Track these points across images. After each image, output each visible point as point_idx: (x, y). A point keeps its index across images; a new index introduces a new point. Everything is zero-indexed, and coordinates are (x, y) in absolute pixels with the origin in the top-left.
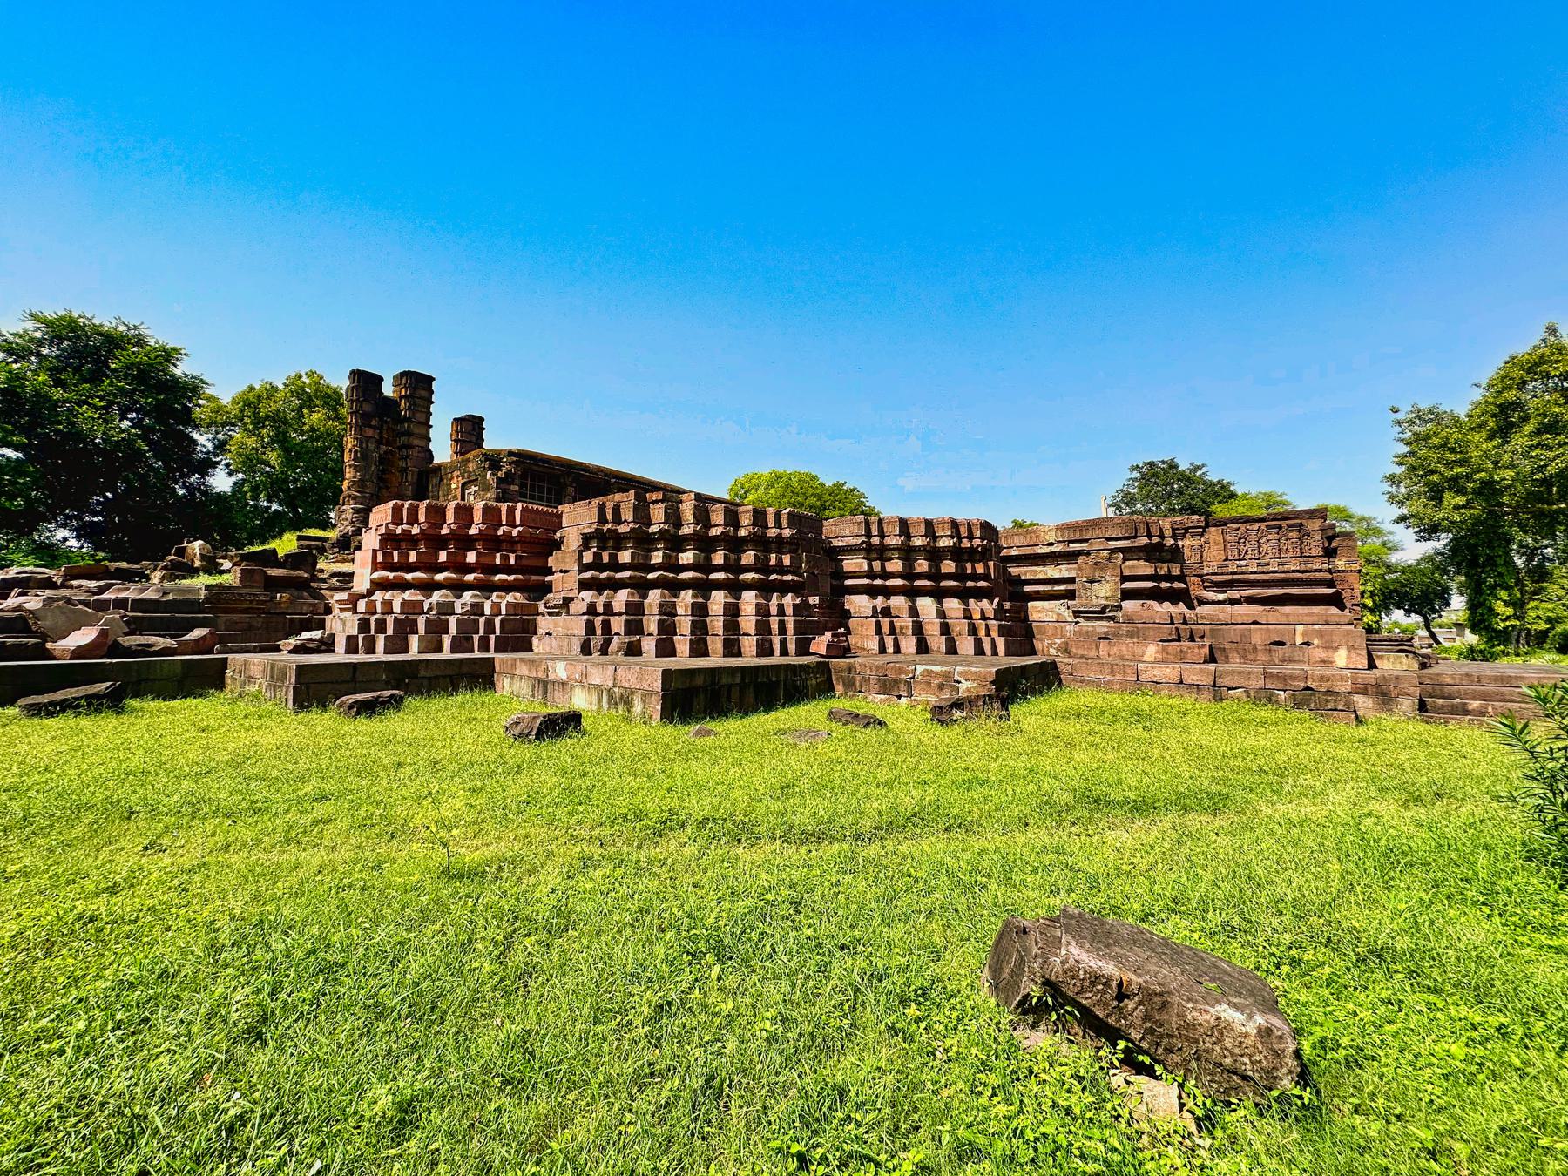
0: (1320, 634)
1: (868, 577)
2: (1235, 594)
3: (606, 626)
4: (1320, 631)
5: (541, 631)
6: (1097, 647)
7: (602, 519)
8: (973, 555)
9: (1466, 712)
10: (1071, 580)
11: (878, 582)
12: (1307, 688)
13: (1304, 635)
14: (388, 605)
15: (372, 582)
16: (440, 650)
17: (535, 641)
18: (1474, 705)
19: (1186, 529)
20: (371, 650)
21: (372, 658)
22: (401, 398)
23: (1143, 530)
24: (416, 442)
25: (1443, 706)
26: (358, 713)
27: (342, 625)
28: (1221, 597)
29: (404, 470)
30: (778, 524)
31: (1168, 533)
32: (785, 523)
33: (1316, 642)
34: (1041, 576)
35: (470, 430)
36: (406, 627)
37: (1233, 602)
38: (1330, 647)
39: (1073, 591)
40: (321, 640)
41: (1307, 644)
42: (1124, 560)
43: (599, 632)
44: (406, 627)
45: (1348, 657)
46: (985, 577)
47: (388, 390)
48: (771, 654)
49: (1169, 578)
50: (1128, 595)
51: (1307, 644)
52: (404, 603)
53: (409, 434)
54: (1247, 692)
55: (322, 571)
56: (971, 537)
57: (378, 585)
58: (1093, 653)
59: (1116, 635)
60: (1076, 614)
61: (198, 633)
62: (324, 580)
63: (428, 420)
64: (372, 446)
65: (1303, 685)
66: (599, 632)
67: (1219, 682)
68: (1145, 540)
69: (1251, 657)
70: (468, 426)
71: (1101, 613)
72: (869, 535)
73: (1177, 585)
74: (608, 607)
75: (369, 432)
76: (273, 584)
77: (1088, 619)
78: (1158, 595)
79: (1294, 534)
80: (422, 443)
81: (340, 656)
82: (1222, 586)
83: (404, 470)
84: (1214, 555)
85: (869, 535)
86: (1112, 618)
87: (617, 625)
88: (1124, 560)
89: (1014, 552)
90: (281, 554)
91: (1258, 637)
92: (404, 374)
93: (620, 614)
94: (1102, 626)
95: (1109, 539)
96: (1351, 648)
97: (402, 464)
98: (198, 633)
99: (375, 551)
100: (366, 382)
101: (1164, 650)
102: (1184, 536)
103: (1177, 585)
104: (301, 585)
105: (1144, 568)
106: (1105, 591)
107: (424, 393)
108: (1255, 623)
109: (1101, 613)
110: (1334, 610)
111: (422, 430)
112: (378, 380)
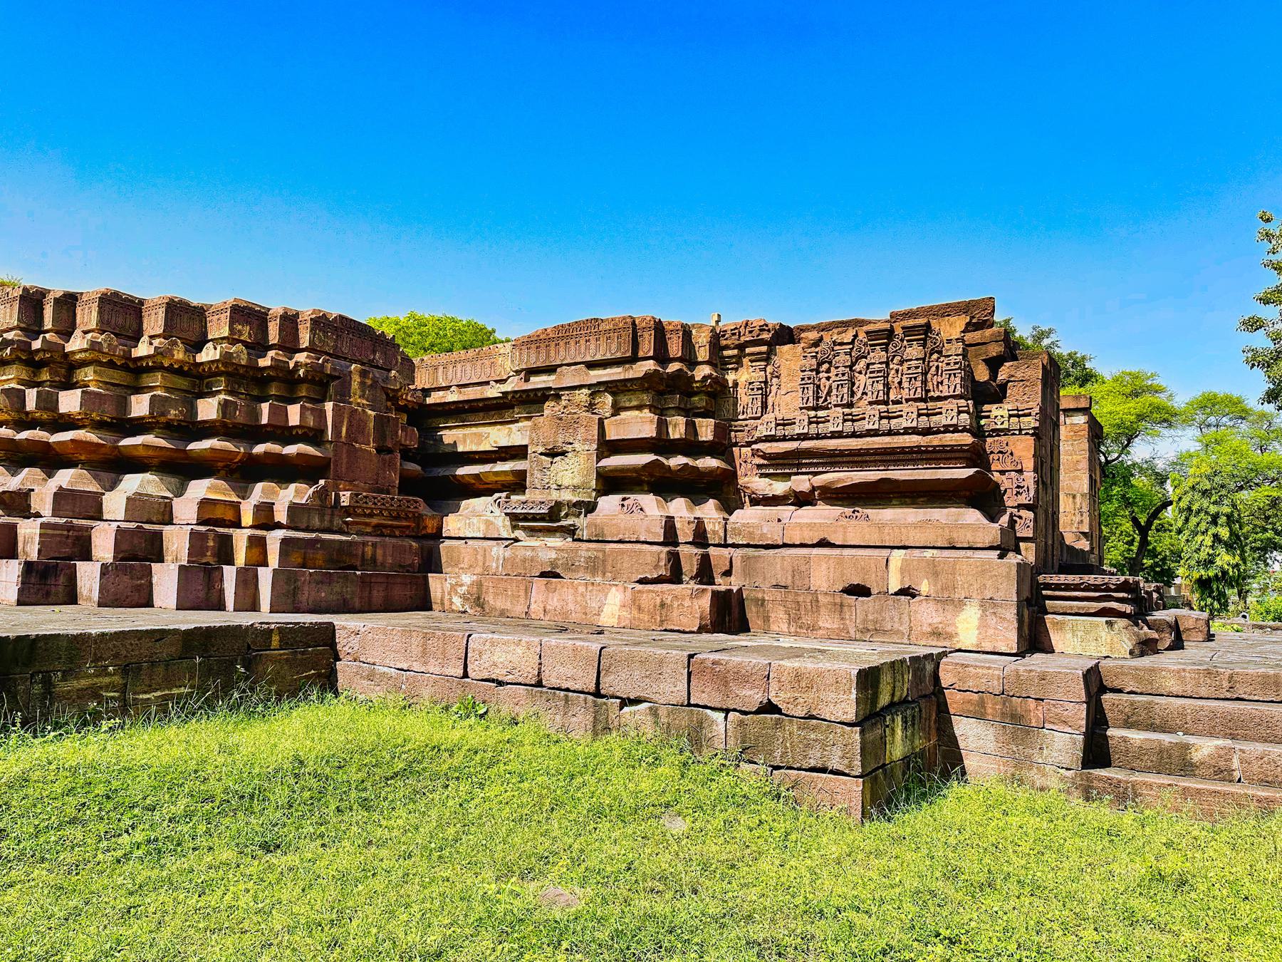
0: (934, 571)
1: (98, 426)
2: (802, 483)
4: (933, 562)
6: (528, 591)
8: (288, 384)
9: (1186, 767)
10: (518, 452)
11: (37, 434)
12: (769, 708)
13: (903, 571)
18: (1204, 748)
19: (742, 347)
21: (246, 619)
23: (647, 347)
25: (1142, 751)
26: (279, 700)
28: (779, 488)
33: (924, 587)
34: (486, 446)
37: (801, 500)
38: (949, 601)
39: (522, 475)
41: (907, 592)
42: (617, 410)
45: (983, 625)
46: (313, 435)
48: (220, 606)
49: (691, 447)
50: (611, 483)
51: (907, 592)
54: (654, 712)
56: (290, 347)
58: (519, 609)
59: (571, 567)
60: (515, 518)
67: (615, 683)
68: (650, 365)
69: (807, 620)
71: (551, 520)
73: (709, 463)
77: (532, 531)
78: (663, 484)
79: (914, 351)
82: (782, 464)
84: (788, 402)
86: (571, 531)
88: (617, 410)
89: (452, 397)
91: (824, 573)
94: (550, 548)
96: (988, 604)
101: (635, 604)
102: (738, 362)
103: (709, 463)
105: (639, 424)
106: (571, 475)
108: (823, 543)
109: (551, 520)
110: (973, 516)
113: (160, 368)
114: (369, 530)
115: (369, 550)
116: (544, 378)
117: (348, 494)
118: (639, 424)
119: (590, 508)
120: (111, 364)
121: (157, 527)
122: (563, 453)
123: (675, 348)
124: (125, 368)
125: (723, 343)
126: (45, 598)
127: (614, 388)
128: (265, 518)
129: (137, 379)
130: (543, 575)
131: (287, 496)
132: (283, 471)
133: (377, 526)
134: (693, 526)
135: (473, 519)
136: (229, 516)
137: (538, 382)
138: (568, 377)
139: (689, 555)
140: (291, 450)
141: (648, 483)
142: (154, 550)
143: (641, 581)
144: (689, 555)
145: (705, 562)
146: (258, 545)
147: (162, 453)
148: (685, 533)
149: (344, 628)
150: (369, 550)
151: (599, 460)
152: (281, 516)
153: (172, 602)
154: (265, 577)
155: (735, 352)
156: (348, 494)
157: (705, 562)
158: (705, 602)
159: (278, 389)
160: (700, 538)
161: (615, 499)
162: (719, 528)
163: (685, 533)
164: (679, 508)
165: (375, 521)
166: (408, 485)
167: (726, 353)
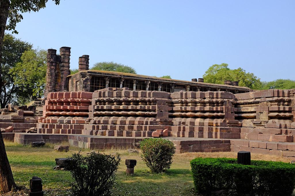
1: (192, 112)
3: (98, 127)
5: (85, 128)
7: (100, 96)
10: (255, 112)
14: (49, 120)
15: (46, 114)
16: (59, 133)
17: (83, 131)
20: (44, 132)
21: (44, 134)
22: (61, 55)
23: (276, 94)
24: (65, 68)
27: (39, 126)
29: (62, 78)
30: (150, 97)
31: (286, 95)
32: (152, 96)
34: (249, 111)
35: (85, 59)
36: (52, 126)
40: (34, 130)
43: (96, 129)
44: (52, 126)
46: (222, 112)
47: (58, 53)
50: (271, 118)
52: (52, 120)
53: (63, 66)
55: (37, 111)
57: (48, 115)
61: (10, 127)
62: (37, 113)
63: (69, 61)
64: (53, 71)
65: (286, 149)
66: (96, 129)
70: (83, 59)
72: (182, 98)
74: (99, 121)
75: (53, 67)
76: (26, 115)
80: (67, 69)
81: (38, 133)
83: (62, 78)
85: (182, 98)
87: (126, 127)
90: (28, 106)
92: (62, 48)
93: (102, 124)
95: (266, 97)
97: (61, 76)
98: (10, 127)
99: (47, 106)
100: (52, 52)
104: (32, 115)
107: (67, 53)
111: (67, 65)
112: (56, 51)
113: (200, 103)
114: (231, 126)
115: (231, 129)
116: (258, 99)
117: (228, 121)
118: (275, 107)
119: (267, 122)
120: (193, 103)
121: (124, 125)
122: (262, 113)
123: (281, 94)
124: (195, 103)
125: (290, 93)
126: (103, 135)
127: (271, 101)
128: (147, 123)
129: (218, 105)
130: (260, 133)
131: (220, 121)
132: (218, 117)
133: (232, 125)
134: (284, 125)
135: (247, 123)
136: (212, 125)
137: (258, 100)
138: (263, 99)
139: (284, 130)
140: (146, 113)
141: (277, 118)
142: (115, 128)
143: (275, 134)
144: (284, 130)
145: (287, 131)
146: (146, 127)
147: (201, 116)
148: (283, 126)
149: (231, 141)
150: (231, 129)
151: (268, 114)
152: (219, 124)
153: (188, 136)
154: (147, 132)
155: (293, 94)
156: (228, 121)
157: (287, 131)
158: (286, 138)
159: (185, 104)
160: (286, 127)
161: (271, 120)
162: (289, 125)
163: (283, 126)
164: (282, 122)
165: (232, 125)
166: (236, 118)
167: (290, 95)
